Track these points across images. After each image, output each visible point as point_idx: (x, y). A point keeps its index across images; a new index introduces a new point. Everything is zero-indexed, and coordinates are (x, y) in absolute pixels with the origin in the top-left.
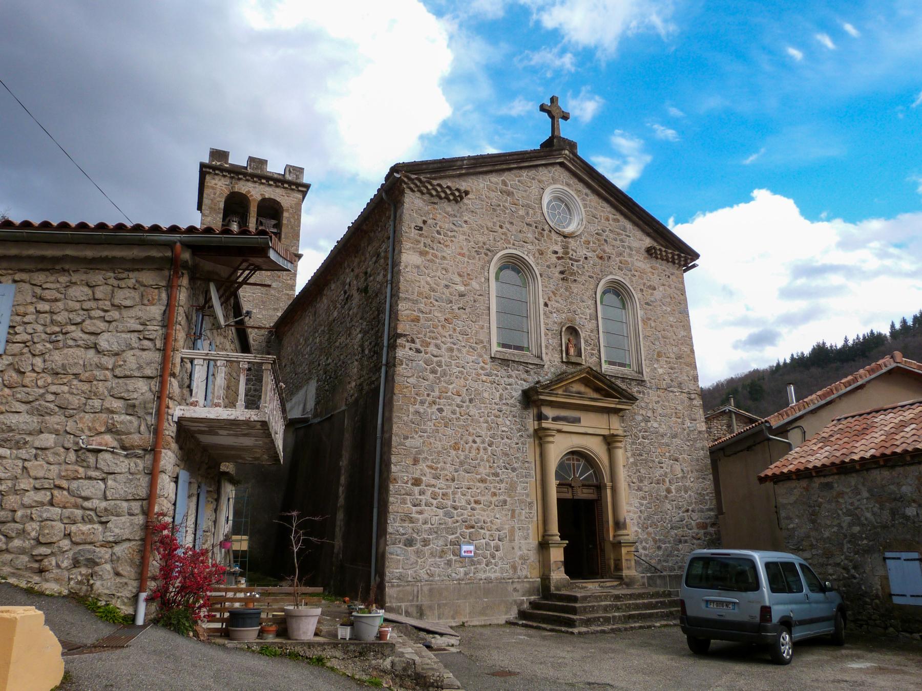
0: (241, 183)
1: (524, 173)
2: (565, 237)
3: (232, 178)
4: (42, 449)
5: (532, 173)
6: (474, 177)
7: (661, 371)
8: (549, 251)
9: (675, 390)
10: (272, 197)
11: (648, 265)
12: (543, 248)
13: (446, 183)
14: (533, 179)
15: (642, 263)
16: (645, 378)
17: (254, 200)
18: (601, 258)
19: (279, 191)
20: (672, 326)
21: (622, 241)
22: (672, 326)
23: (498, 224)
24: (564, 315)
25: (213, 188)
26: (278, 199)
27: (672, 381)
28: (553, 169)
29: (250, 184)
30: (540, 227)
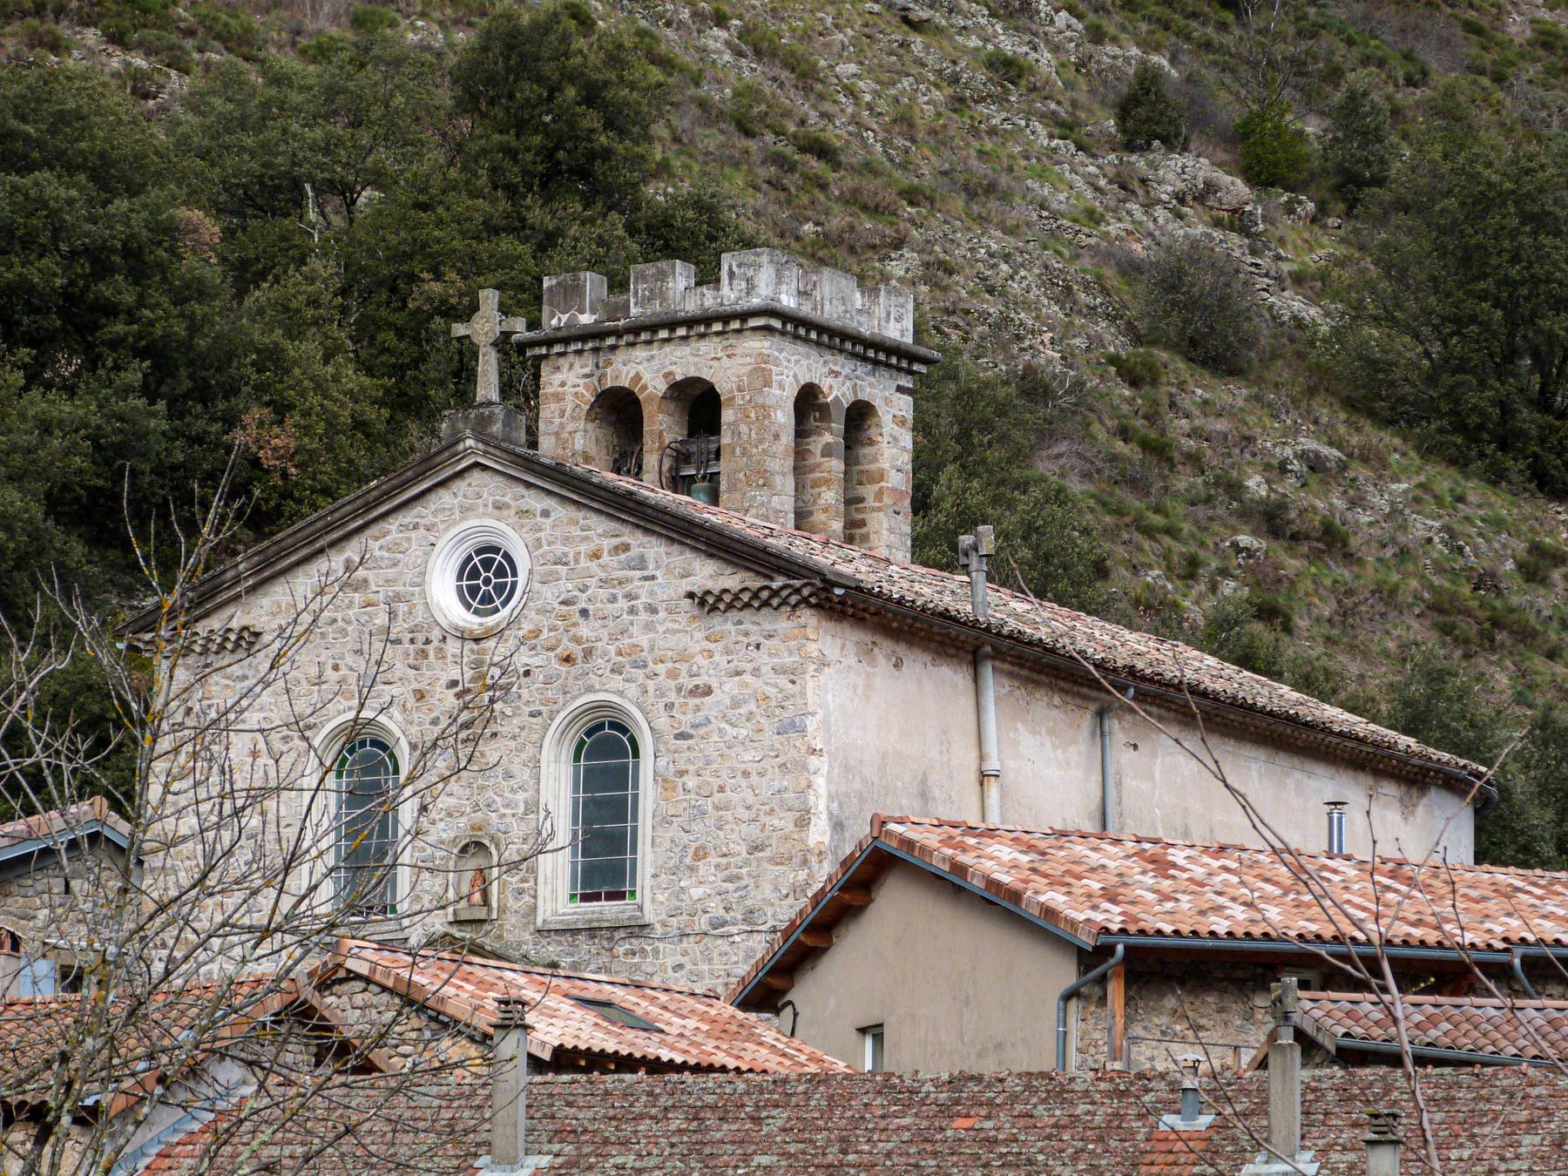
0: (619, 357)
1: (393, 524)
2: (477, 640)
3: (596, 350)
4: (1335, 804)
5: (406, 517)
6: (282, 579)
7: (696, 893)
8: (440, 688)
9: (734, 930)
10: (693, 373)
11: (699, 635)
12: (423, 686)
13: (215, 623)
14: (416, 527)
15: (687, 635)
16: (649, 916)
17: (650, 398)
18: (568, 659)
19: (709, 347)
20: (746, 774)
21: (630, 597)
22: (746, 774)
23: (330, 662)
24: (464, 820)
25: (558, 398)
26: (706, 375)
27: (727, 909)
28: (460, 486)
29: (640, 353)
30: (420, 638)
